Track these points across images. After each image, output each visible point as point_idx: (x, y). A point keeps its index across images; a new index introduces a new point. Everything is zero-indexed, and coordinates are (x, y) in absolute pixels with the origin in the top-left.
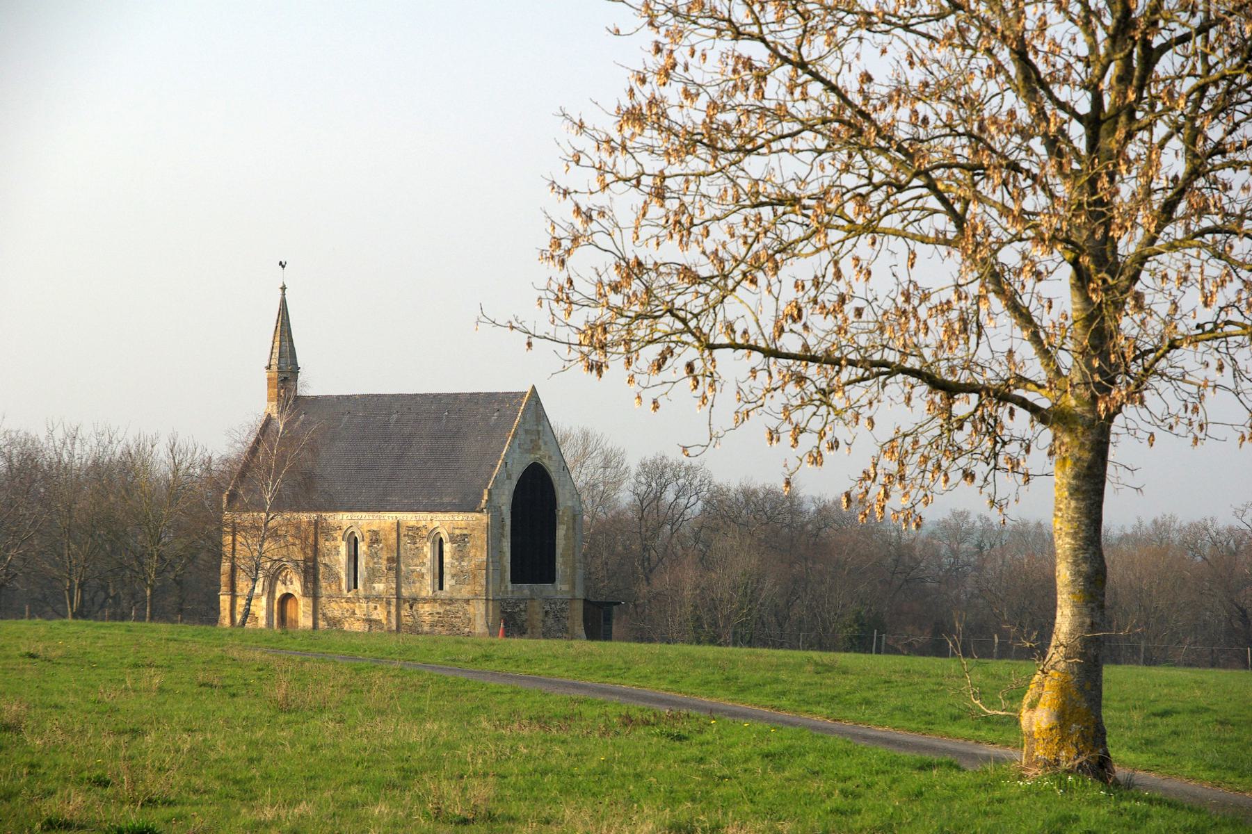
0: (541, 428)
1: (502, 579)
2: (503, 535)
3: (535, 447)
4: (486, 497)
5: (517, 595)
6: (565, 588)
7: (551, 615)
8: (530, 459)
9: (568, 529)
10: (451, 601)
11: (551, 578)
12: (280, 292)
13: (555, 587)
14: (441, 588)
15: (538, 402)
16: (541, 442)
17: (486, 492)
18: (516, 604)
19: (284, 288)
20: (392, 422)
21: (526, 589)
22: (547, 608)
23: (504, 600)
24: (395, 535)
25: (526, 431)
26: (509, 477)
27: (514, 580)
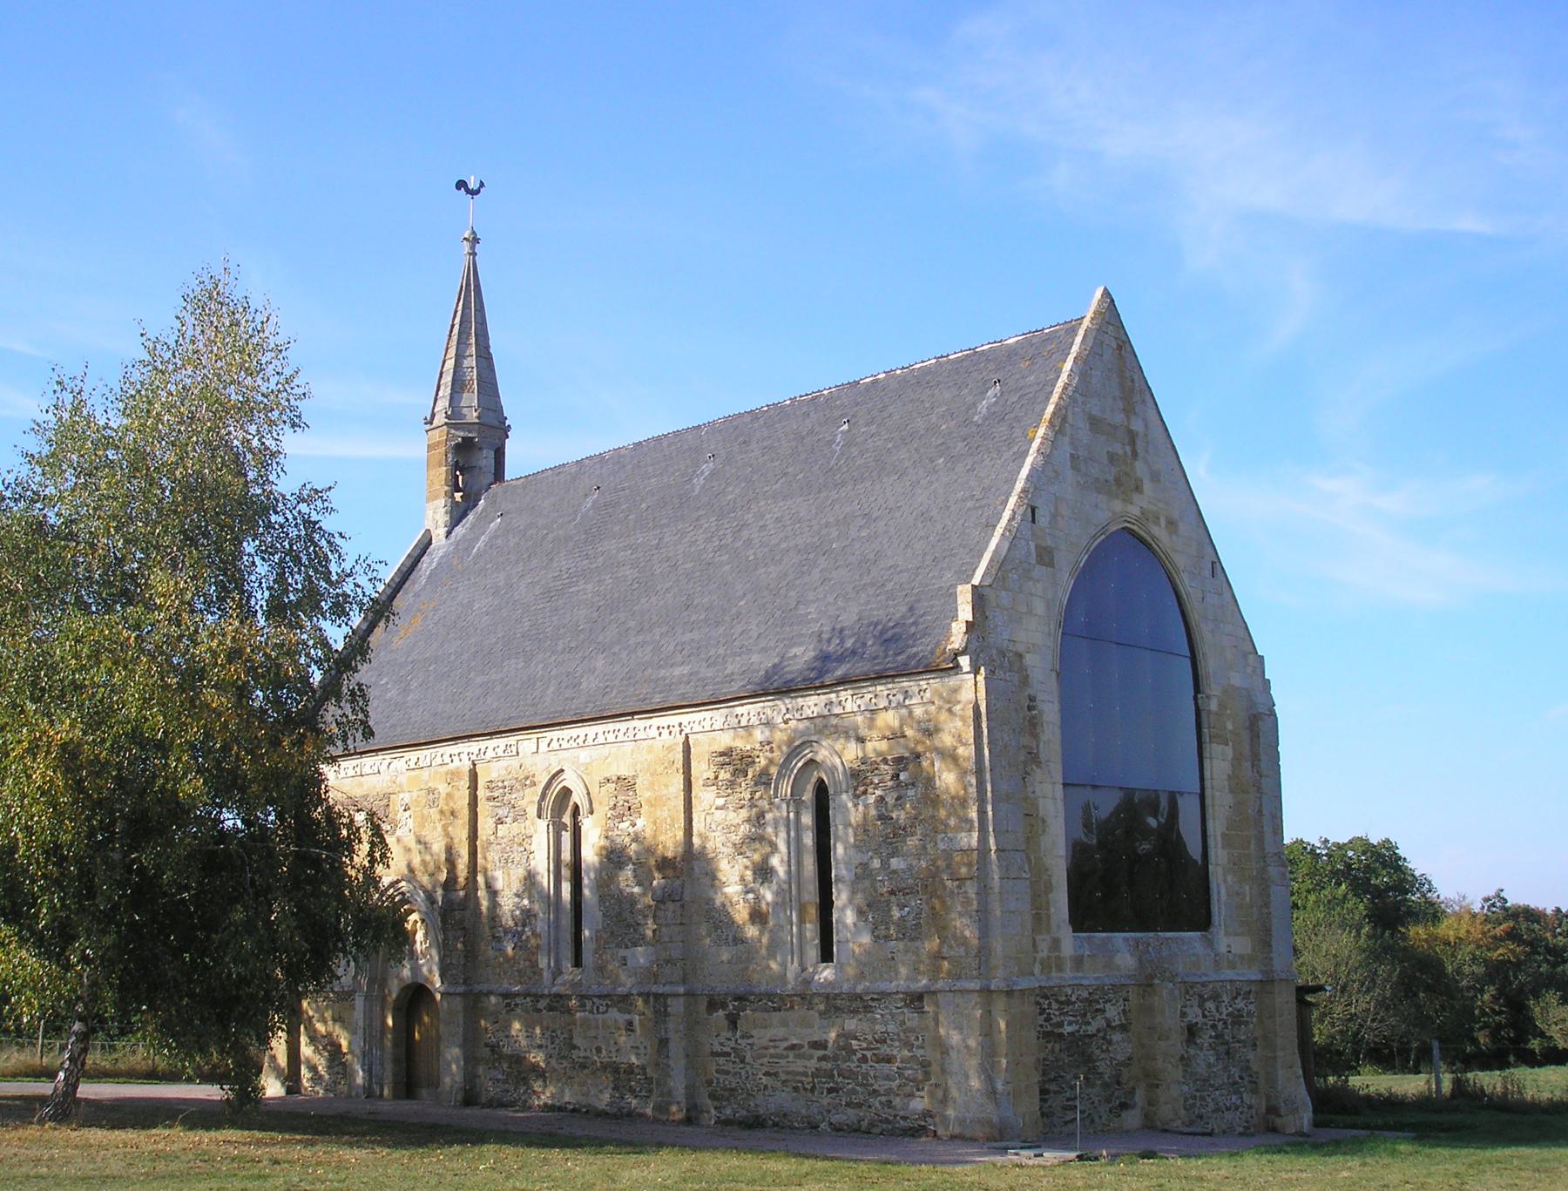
0: (1137, 425)
1: (1040, 918)
2: (1033, 757)
3: (1125, 485)
4: (965, 612)
5: (1092, 976)
6: (1241, 945)
7: (1205, 1039)
8: (1110, 512)
9: (1237, 760)
10: (859, 1003)
11: (1201, 920)
12: (466, 246)
13: (1210, 943)
14: (826, 955)
15: (1123, 345)
16: (1140, 468)
17: (964, 596)
18: (1092, 1004)
19: (475, 240)
20: (699, 482)
21: (1122, 951)
22: (1194, 1015)
23: (1045, 994)
24: (678, 781)
25: (1095, 423)
26: (1045, 556)
27: (1085, 916)
